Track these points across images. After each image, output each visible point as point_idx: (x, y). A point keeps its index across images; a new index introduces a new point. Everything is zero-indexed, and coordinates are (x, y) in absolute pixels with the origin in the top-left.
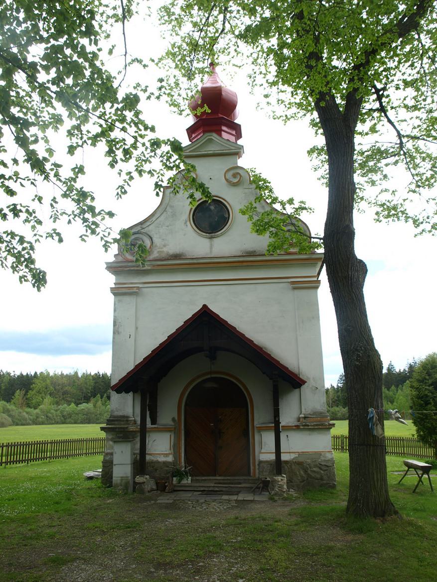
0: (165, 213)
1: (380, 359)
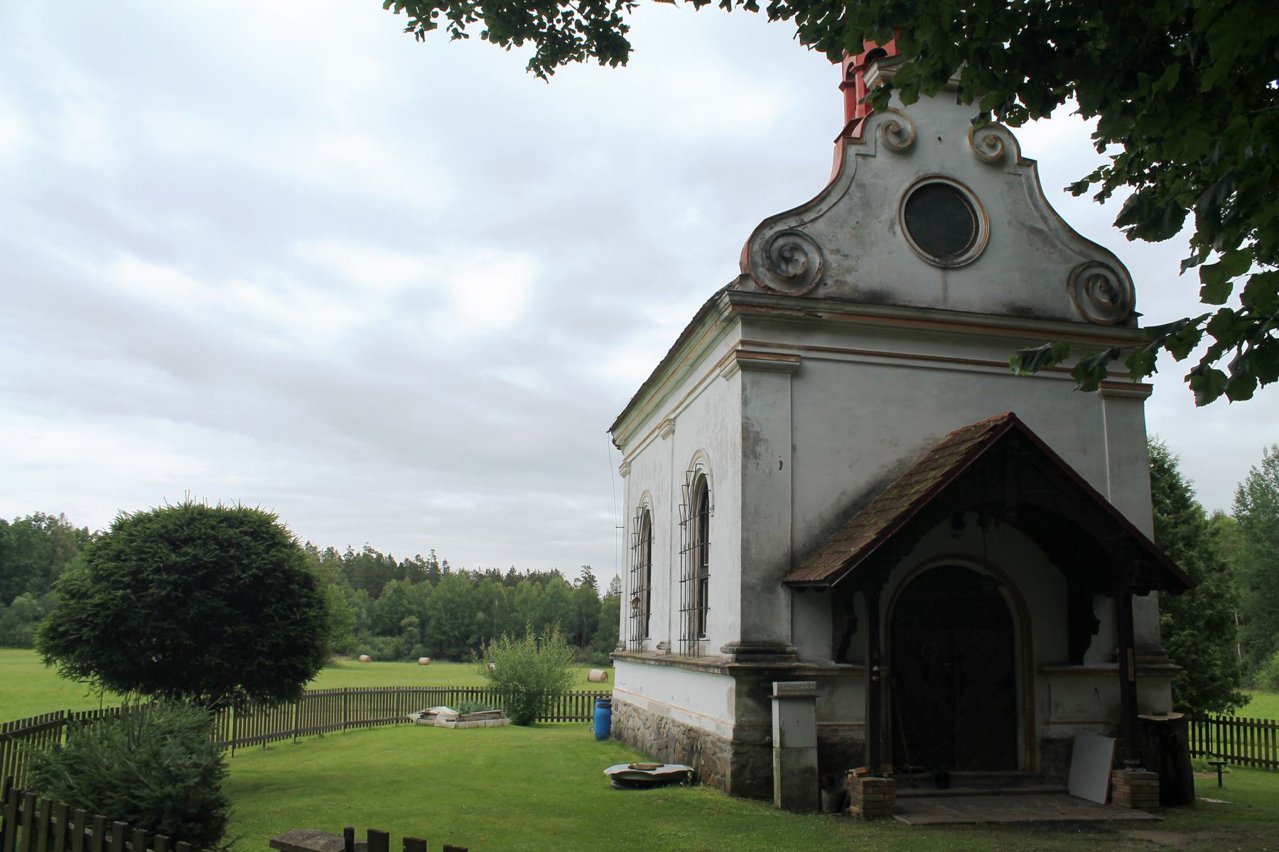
0: (847, 197)
1: (1084, 653)
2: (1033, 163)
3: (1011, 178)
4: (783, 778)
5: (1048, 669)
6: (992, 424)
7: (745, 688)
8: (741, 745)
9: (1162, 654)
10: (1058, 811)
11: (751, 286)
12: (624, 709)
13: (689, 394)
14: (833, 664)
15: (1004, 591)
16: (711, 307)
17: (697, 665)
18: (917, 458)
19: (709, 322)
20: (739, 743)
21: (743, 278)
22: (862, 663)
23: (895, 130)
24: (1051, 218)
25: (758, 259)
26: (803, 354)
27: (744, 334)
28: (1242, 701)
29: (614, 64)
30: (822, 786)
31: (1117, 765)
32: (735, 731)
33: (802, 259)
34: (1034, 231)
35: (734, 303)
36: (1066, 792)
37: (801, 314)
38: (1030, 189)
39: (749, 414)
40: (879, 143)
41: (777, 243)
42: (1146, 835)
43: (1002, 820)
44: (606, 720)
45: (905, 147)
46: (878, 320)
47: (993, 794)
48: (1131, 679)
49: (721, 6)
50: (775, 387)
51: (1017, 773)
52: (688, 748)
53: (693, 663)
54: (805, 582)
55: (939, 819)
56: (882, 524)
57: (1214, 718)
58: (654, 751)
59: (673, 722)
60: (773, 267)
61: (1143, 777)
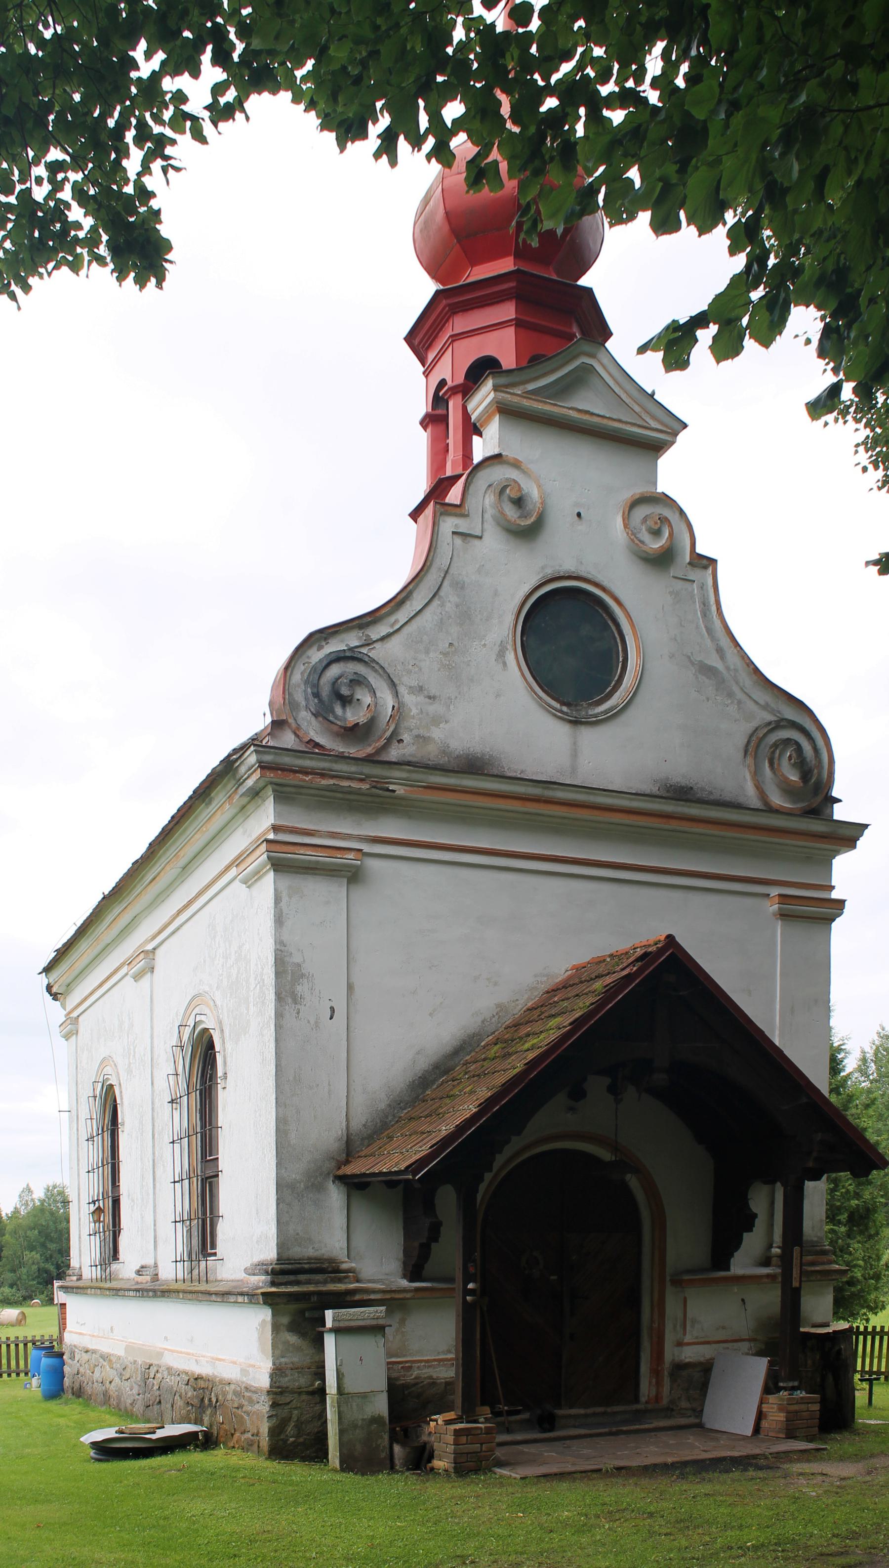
0: (436, 602)
2: (713, 562)
3: (679, 585)
4: (341, 1432)
5: (686, 1277)
6: (639, 952)
7: (285, 1320)
8: (281, 1393)
9: (824, 1253)
10: (696, 1448)
11: (288, 740)
12: (86, 1357)
13: (180, 912)
14: (405, 1283)
15: (633, 1181)
16: (226, 770)
17: (210, 1294)
18: (525, 1000)
19: (219, 796)
20: (278, 1392)
21: (277, 725)
22: (451, 1280)
23: (515, 495)
24: (730, 651)
25: (299, 697)
26: (366, 848)
27: (277, 814)
28: (876, 1308)
29: (141, 282)
30: (397, 1438)
31: (771, 1387)
32: (272, 1376)
33: (367, 700)
34: (707, 670)
35: (263, 766)
36: (700, 1426)
37: (364, 786)
38: (705, 604)
39: (285, 937)
40: (488, 516)
41: (333, 669)
42: (807, 1467)
43: (634, 1463)
44: (58, 1374)
45: (527, 528)
46: (476, 797)
47: (611, 1434)
48: (795, 1284)
49: (377, 155)
50: (323, 897)
51: (639, 1407)
52: (196, 1402)
53: (198, 1288)
54: (374, 1175)
55: (554, 1469)
56: (484, 1093)
57: (862, 1329)
58: (139, 1408)
59: (169, 1369)
60: (322, 713)
61: (802, 1401)
